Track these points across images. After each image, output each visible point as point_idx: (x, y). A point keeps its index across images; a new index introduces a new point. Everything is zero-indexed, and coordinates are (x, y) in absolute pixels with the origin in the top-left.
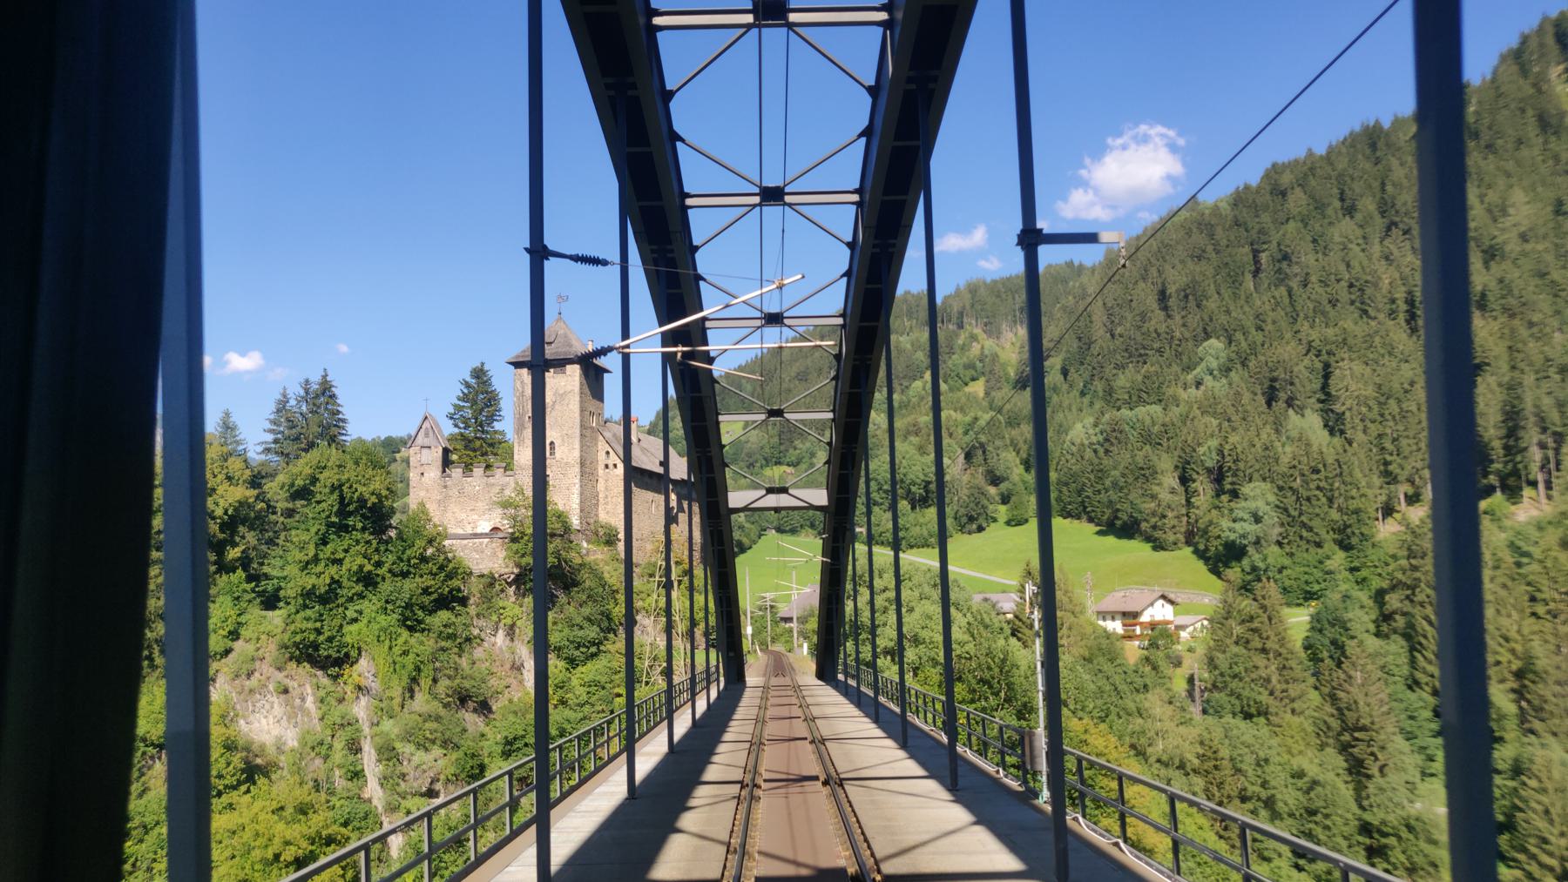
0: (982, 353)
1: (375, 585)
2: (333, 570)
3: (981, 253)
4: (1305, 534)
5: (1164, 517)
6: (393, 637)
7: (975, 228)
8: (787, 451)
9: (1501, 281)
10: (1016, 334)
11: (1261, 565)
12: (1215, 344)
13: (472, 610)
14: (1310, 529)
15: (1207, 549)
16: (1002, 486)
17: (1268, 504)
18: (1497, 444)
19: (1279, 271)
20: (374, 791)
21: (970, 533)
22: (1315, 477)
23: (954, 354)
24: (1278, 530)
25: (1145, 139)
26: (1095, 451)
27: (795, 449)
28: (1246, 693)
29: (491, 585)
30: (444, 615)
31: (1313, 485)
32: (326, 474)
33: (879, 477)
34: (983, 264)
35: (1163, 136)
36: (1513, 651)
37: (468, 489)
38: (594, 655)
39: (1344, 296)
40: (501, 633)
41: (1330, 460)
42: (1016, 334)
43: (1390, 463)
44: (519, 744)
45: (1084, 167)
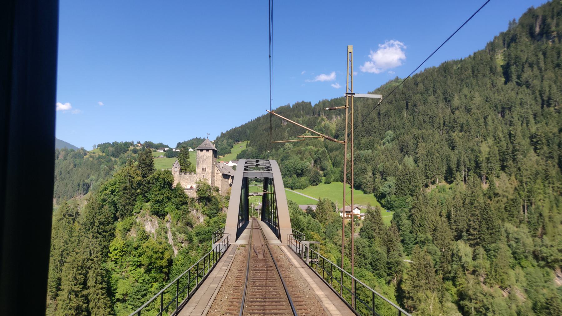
0: (325, 125)
1: (170, 199)
2: (162, 196)
3: (333, 82)
4: (402, 191)
5: (367, 184)
6: (175, 211)
9: (467, 121)
11: (390, 200)
12: (390, 132)
13: (189, 205)
14: (404, 191)
15: (377, 195)
16: (325, 171)
18: (454, 169)
19: (413, 110)
20: (171, 242)
21: (314, 185)
24: (395, 190)
25: (392, 45)
28: (370, 233)
29: (193, 200)
30: (184, 206)
31: (405, 178)
32: (161, 176)
34: (333, 85)
35: (399, 45)
36: (433, 224)
37: (185, 177)
38: (215, 216)
39: (428, 120)
40: (195, 211)
41: (411, 171)
44: (200, 234)
45: (370, 54)
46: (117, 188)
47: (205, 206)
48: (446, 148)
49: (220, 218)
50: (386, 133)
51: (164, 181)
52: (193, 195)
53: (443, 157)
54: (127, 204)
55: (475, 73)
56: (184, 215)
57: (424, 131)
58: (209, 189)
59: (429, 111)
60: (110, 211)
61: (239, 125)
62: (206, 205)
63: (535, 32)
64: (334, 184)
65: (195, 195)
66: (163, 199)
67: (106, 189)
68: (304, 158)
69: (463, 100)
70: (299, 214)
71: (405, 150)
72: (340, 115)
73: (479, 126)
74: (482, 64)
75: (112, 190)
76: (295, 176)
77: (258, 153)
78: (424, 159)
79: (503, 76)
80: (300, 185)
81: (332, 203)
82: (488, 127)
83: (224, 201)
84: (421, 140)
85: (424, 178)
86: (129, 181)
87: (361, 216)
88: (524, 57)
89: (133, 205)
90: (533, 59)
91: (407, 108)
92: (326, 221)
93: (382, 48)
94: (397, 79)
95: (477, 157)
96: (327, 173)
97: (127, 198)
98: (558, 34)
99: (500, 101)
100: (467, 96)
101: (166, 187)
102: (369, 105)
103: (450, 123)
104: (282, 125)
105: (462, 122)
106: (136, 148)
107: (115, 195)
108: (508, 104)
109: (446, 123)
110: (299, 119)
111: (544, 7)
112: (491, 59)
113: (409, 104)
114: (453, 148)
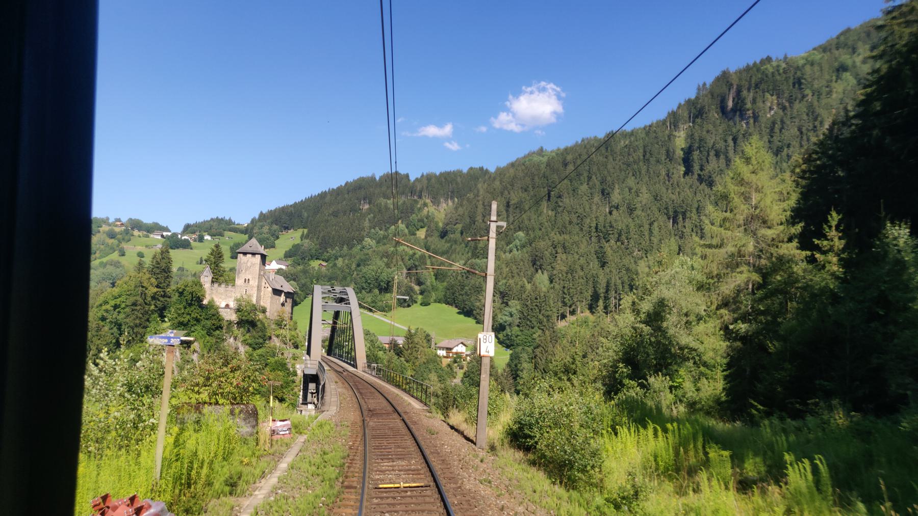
0: (428, 214)
3: (449, 140)
4: (528, 323)
6: (205, 337)
7: (446, 125)
8: (323, 253)
9: (627, 226)
10: (448, 205)
11: (510, 334)
12: (521, 234)
13: (224, 331)
14: (531, 322)
16: (422, 286)
17: (517, 310)
18: (602, 295)
19: (556, 202)
21: (404, 307)
22: (535, 301)
23: (414, 213)
24: (518, 320)
25: (544, 90)
26: (463, 276)
27: (327, 252)
29: (230, 324)
30: (218, 332)
31: (534, 304)
32: (187, 289)
33: (367, 276)
34: (447, 144)
35: (554, 90)
38: (261, 347)
39: (575, 220)
40: (232, 338)
41: (542, 295)
42: (448, 205)
43: (565, 298)
45: (508, 101)
46: (123, 302)
47: (247, 333)
48: (595, 264)
49: (268, 350)
50: (515, 235)
51: (192, 295)
52: (230, 316)
53: (589, 276)
54: (136, 326)
55: (647, 155)
56: (217, 344)
57: (567, 237)
58: (254, 309)
59: (578, 207)
60: (112, 334)
61: (291, 203)
62: (249, 331)
63: (727, 106)
64: (435, 307)
65: (234, 317)
66: (189, 321)
67: (106, 302)
68: (392, 265)
69: (625, 195)
70: (377, 349)
71: (538, 263)
72: (452, 198)
73: (642, 235)
74: (657, 143)
75: (116, 304)
76: (376, 291)
77: (320, 251)
78: (562, 278)
79: (683, 165)
80: (384, 305)
81: (428, 335)
82: (652, 238)
83: (273, 326)
84: (560, 250)
85: (560, 304)
86: (142, 294)
87: (467, 355)
88: (710, 141)
89: (145, 327)
90: (721, 145)
91: (549, 200)
92: (416, 361)
93: (526, 92)
94: (541, 152)
95: (633, 279)
96: (425, 289)
97: (137, 317)
98: (753, 113)
99: (673, 201)
100: (632, 189)
101: (194, 305)
102: (495, 190)
103: (604, 227)
104: (361, 207)
105: (620, 228)
106: (113, 230)
107: (119, 312)
108: (682, 206)
109: (599, 227)
110: (388, 202)
111: (740, 72)
112: (669, 136)
113: (552, 193)
114: (603, 265)
